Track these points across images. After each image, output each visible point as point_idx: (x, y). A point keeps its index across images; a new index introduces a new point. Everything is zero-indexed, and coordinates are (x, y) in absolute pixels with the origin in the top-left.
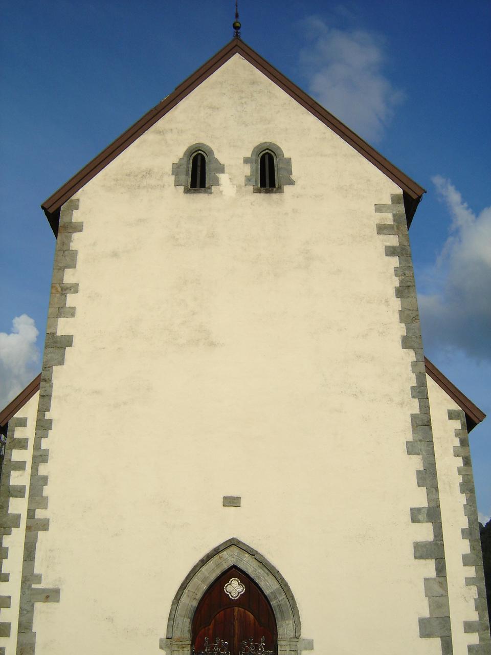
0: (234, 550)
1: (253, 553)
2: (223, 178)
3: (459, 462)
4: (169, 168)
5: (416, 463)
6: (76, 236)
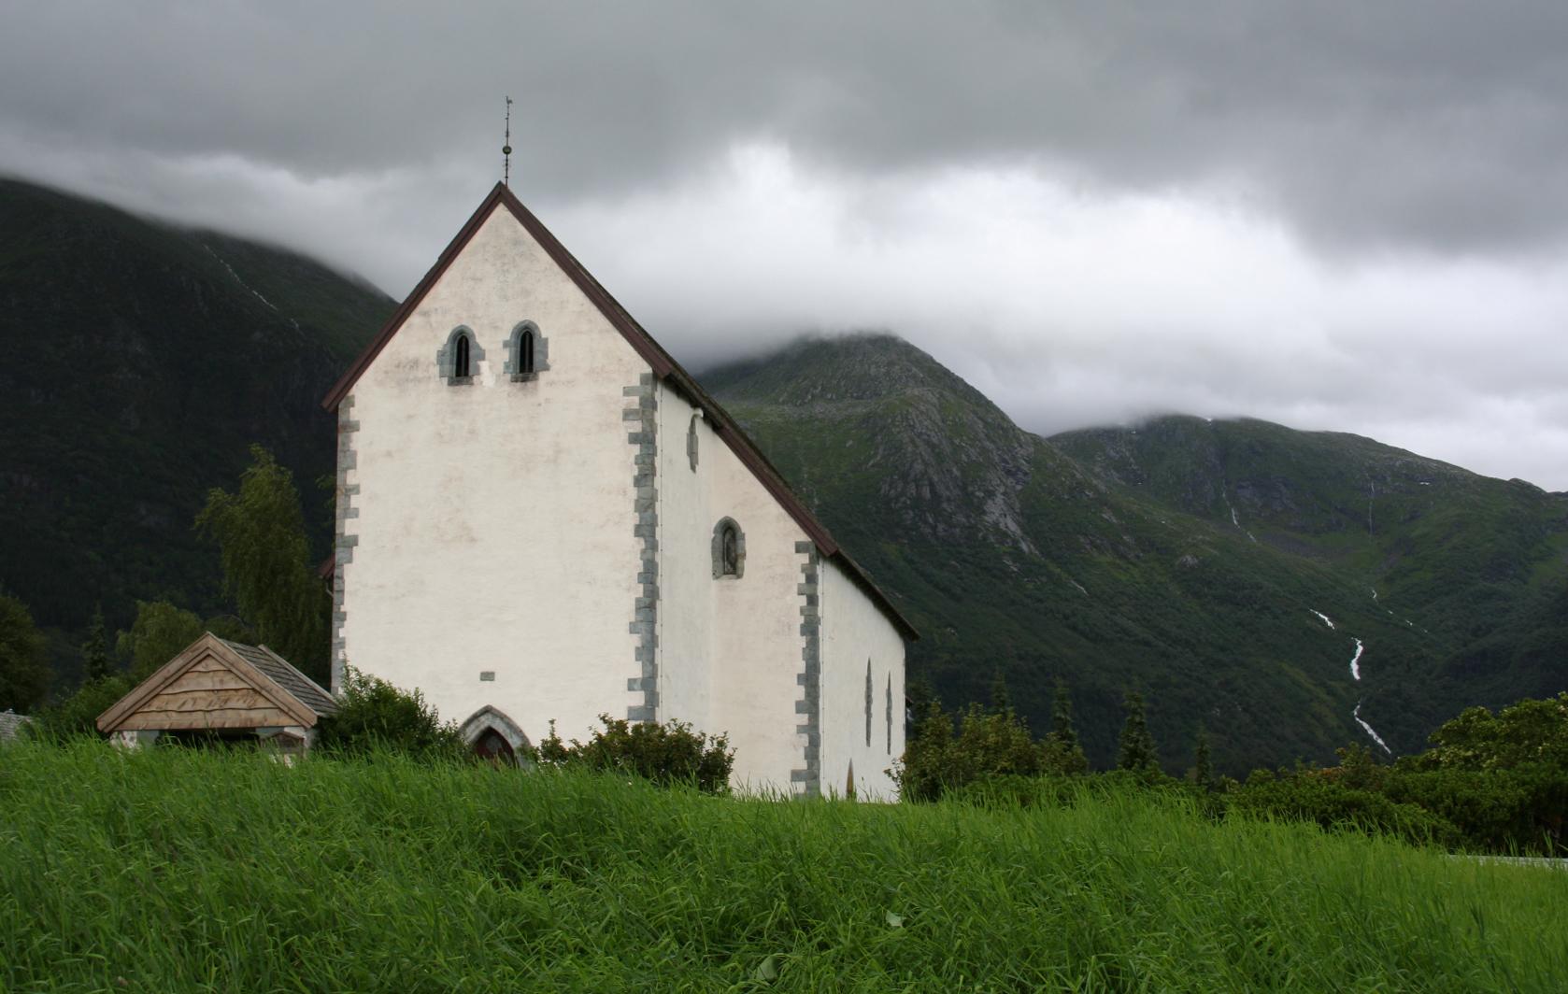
0: (489, 716)
1: (503, 717)
2: (484, 365)
3: (803, 601)
4: (433, 358)
5: (636, 641)
6: (355, 435)
